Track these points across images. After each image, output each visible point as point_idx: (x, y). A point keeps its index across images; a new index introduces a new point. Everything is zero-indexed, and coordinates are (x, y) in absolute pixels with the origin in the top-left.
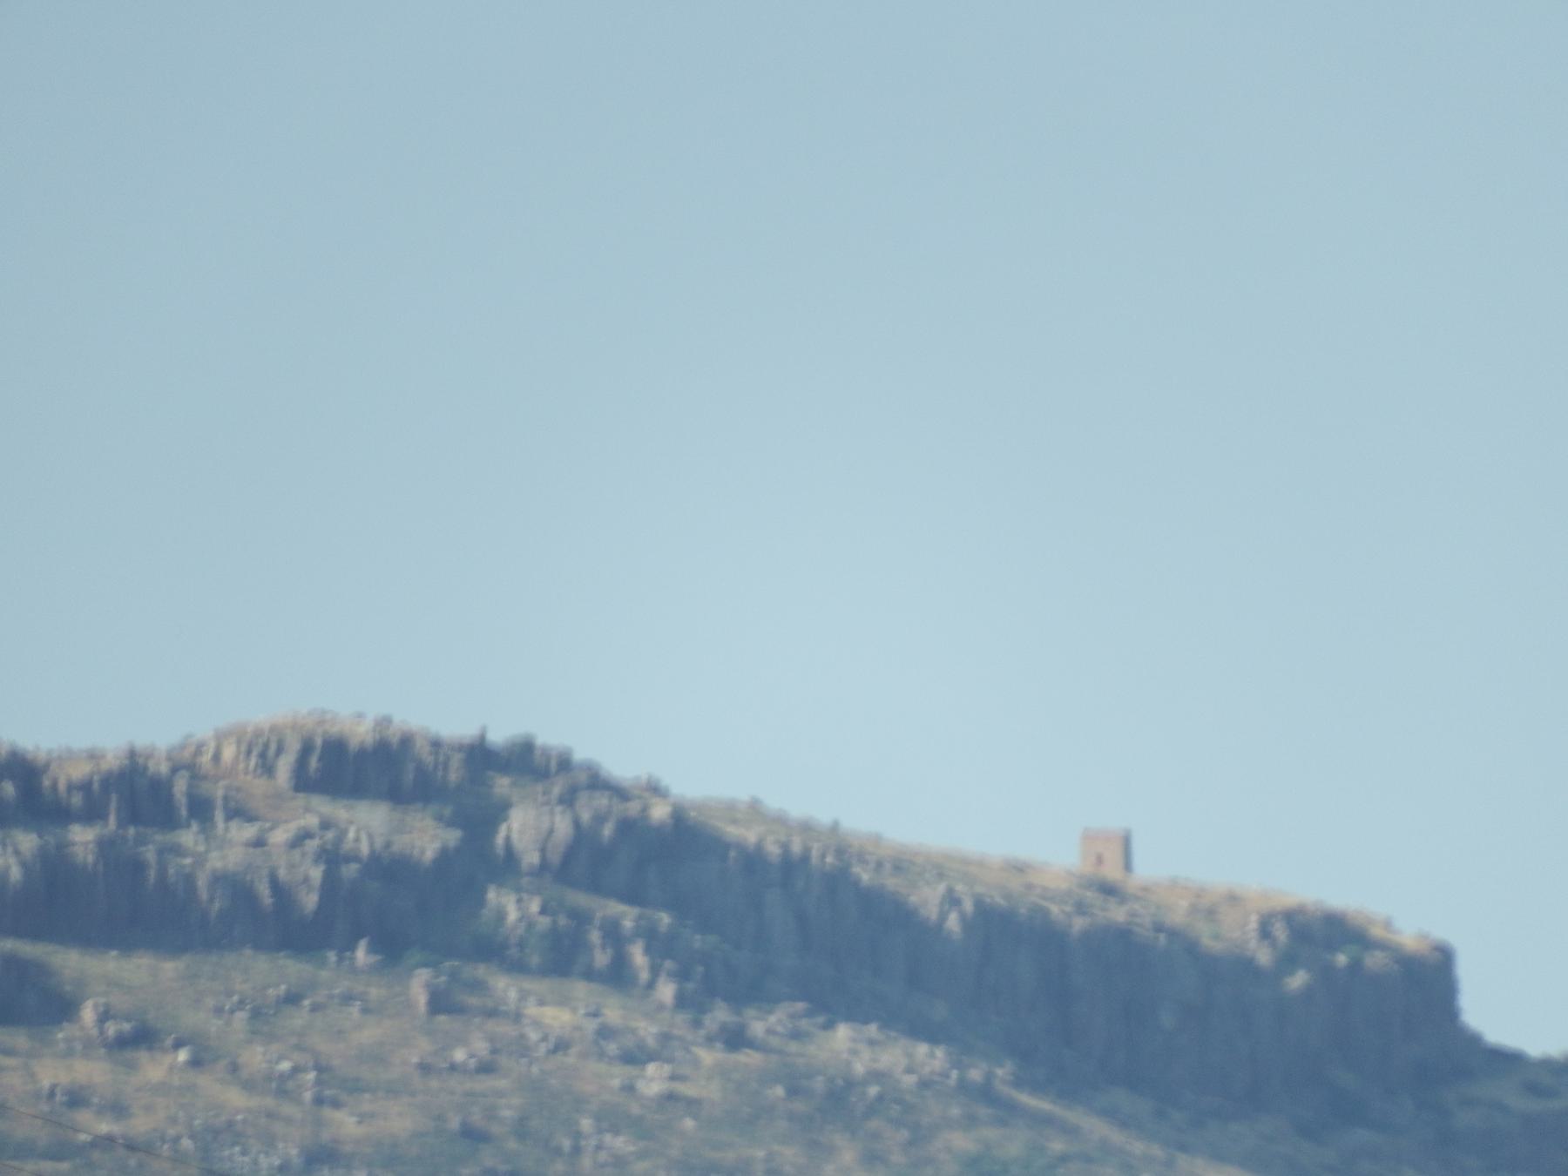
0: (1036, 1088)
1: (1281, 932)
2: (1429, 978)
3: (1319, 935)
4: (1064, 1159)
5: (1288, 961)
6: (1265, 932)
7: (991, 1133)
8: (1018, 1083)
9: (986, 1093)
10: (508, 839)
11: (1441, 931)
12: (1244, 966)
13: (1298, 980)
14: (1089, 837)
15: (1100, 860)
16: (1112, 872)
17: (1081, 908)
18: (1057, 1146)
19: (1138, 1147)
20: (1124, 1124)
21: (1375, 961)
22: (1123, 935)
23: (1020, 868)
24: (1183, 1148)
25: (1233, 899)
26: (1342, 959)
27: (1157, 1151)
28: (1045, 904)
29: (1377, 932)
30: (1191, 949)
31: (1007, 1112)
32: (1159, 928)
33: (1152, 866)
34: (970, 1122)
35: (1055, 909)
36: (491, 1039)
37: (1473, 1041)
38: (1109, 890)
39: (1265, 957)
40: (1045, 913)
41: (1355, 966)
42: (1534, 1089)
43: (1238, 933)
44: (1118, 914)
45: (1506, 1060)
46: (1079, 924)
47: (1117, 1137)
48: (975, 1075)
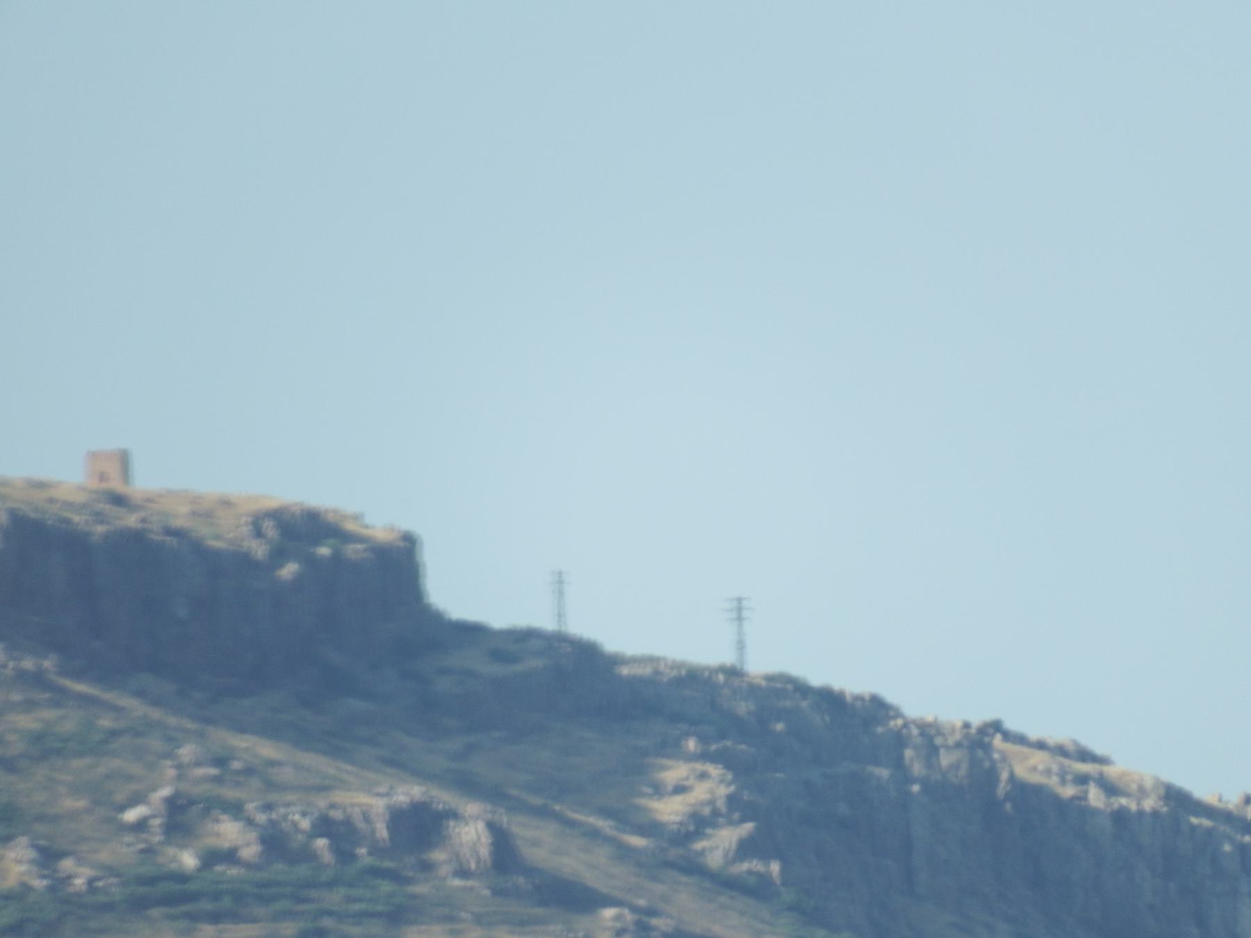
0: (79, 675)
1: (269, 528)
2: (398, 563)
3: (302, 529)
4: (114, 734)
5: (279, 555)
6: (259, 533)
7: (49, 714)
8: (64, 673)
9: (37, 680)
10: (1012, 777)
11: (406, 525)
12: (243, 561)
13: (289, 570)
14: (94, 456)
15: (102, 477)
16: (116, 485)
17: (100, 517)
18: (106, 722)
19: (172, 720)
20: (157, 702)
21: (353, 551)
22: (137, 537)
23: (41, 485)
24: (208, 721)
25: (226, 503)
26: (324, 551)
27: (190, 725)
28: (68, 515)
29: (350, 526)
30: (198, 548)
31: (61, 697)
32: (169, 532)
33: (146, 480)
34: (30, 706)
35: (76, 518)
36: (501, 840)
37: (435, 619)
38: (119, 500)
39: (259, 550)
40: (68, 521)
41: (337, 557)
42: (499, 656)
43: (228, 534)
44: (131, 521)
45: (472, 632)
46: (100, 529)
47: (156, 714)
48: (28, 664)
